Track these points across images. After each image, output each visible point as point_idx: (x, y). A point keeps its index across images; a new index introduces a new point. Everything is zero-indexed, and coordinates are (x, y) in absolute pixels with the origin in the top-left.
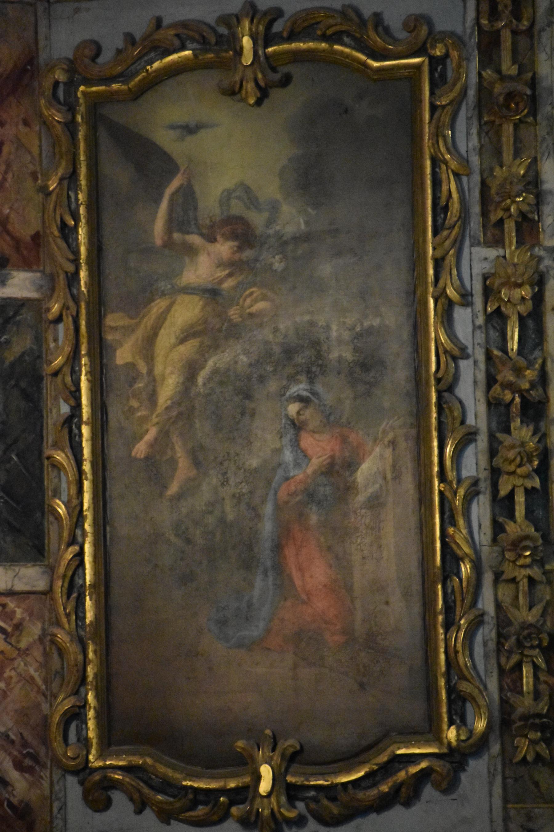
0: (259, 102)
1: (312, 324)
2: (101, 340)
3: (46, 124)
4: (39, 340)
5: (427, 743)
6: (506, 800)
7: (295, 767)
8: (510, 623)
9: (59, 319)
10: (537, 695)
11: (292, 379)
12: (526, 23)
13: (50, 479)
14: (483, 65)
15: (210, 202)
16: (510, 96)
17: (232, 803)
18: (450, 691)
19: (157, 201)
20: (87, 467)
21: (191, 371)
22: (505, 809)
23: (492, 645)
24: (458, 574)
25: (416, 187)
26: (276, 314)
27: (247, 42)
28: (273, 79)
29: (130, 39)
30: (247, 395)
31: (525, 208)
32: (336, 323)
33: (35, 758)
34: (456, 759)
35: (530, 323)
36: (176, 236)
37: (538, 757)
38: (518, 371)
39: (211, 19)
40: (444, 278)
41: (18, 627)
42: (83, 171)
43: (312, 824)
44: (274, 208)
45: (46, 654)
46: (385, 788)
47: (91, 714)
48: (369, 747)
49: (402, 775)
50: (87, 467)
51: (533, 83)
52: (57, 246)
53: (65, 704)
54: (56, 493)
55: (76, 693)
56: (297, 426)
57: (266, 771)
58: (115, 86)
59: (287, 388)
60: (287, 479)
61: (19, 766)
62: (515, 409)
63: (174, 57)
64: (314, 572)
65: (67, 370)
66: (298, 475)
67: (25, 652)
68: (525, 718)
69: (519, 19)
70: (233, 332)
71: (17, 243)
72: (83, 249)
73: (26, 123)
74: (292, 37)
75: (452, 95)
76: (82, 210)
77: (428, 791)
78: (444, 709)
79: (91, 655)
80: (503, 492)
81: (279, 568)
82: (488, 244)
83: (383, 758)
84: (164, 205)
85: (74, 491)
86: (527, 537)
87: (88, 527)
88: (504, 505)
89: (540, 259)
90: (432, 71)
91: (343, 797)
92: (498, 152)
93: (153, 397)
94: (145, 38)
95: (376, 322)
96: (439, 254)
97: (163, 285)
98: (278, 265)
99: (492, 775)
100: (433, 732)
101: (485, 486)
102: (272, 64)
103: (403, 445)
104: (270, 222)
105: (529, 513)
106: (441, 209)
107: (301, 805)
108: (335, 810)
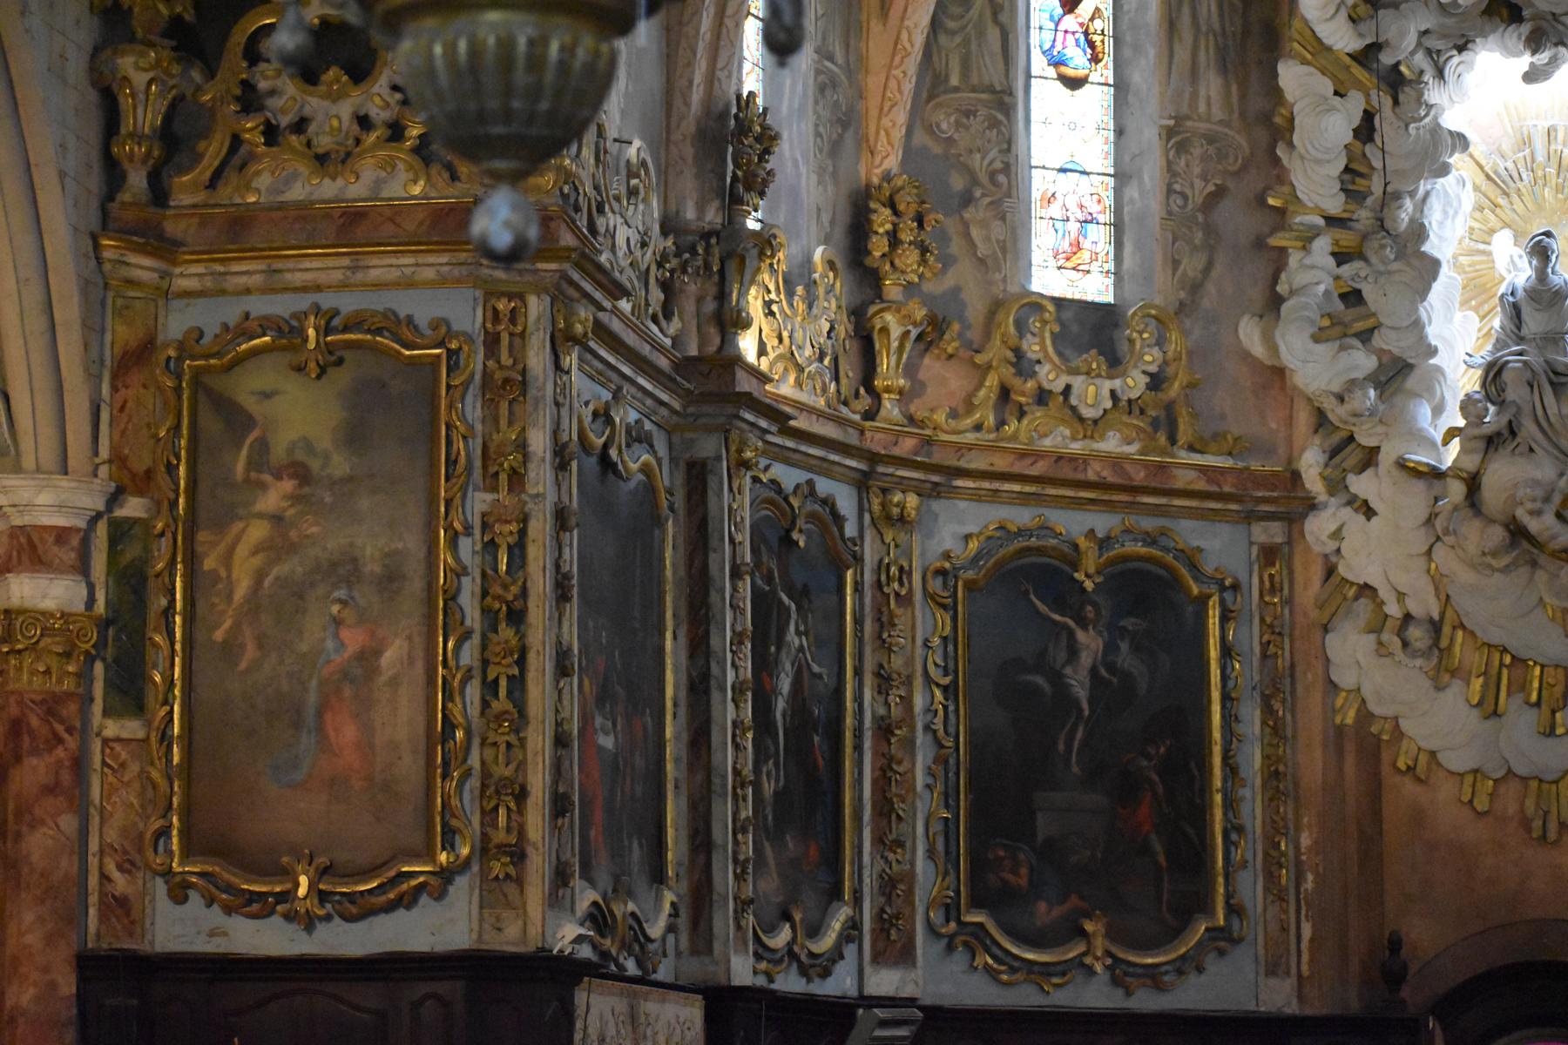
0: (319, 377)
1: (351, 545)
2: (193, 552)
3: (160, 389)
4: (147, 549)
5: (425, 863)
6: (481, 907)
7: (325, 878)
8: (491, 776)
9: (162, 534)
10: (509, 830)
11: (335, 586)
12: (520, 328)
13: (150, 653)
14: (487, 357)
15: (279, 452)
16: (506, 381)
17: (278, 903)
18: (443, 827)
19: (239, 446)
20: (178, 647)
21: (260, 576)
22: (481, 913)
23: (477, 793)
24: (454, 738)
25: (433, 438)
26: (325, 537)
27: (311, 332)
28: (331, 359)
29: (226, 327)
30: (301, 596)
31: (515, 465)
32: (371, 546)
33: (133, 864)
34: (446, 876)
35: (516, 551)
36: (253, 475)
37: (507, 876)
38: (505, 587)
39: (287, 316)
40: (453, 513)
41: (123, 765)
42: (185, 422)
43: (337, 920)
44: (327, 457)
45: (143, 787)
46: (391, 896)
47: (175, 832)
48: (385, 864)
49: (405, 887)
50: (178, 647)
51: (524, 372)
52: (162, 477)
53: (158, 824)
54: (155, 666)
55: (164, 816)
56: (337, 622)
57: (303, 880)
58: (212, 361)
59: (331, 592)
60: (328, 662)
61: (120, 868)
62: (502, 615)
63: (257, 341)
64: (346, 732)
65: (166, 573)
66: (337, 659)
67: (128, 784)
68: (499, 847)
69: (515, 325)
70: (293, 548)
71: (134, 476)
72: (182, 483)
73: (145, 386)
74: (345, 329)
75: (463, 378)
76: (183, 453)
77: (424, 899)
78: (439, 839)
79: (176, 788)
80: (491, 677)
81: (320, 729)
82: (486, 490)
83: (392, 873)
84: (244, 452)
85: (168, 664)
86: (506, 712)
87: (177, 692)
88: (491, 687)
89: (525, 503)
90: (449, 359)
91: (360, 900)
92: (496, 420)
93: (229, 597)
94: (238, 326)
95: (400, 545)
96: (451, 494)
97: (241, 511)
98: (328, 499)
99: (472, 889)
100: (431, 857)
101: (477, 673)
102: (330, 349)
103: (417, 640)
104: (324, 466)
105: (510, 693)
106: (451, 462)
107: (329, 906)
108: (354, 910)
